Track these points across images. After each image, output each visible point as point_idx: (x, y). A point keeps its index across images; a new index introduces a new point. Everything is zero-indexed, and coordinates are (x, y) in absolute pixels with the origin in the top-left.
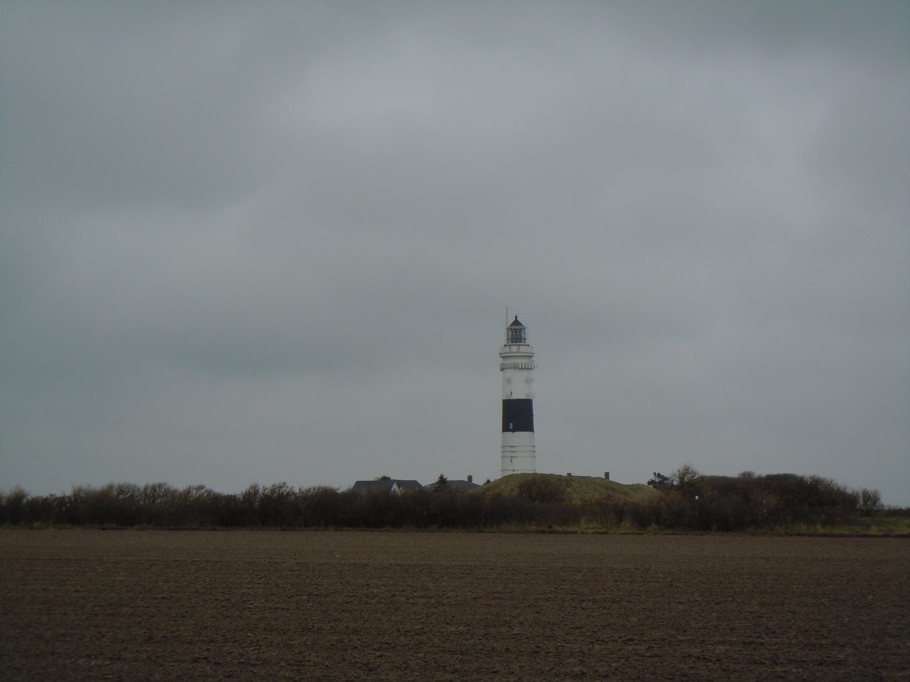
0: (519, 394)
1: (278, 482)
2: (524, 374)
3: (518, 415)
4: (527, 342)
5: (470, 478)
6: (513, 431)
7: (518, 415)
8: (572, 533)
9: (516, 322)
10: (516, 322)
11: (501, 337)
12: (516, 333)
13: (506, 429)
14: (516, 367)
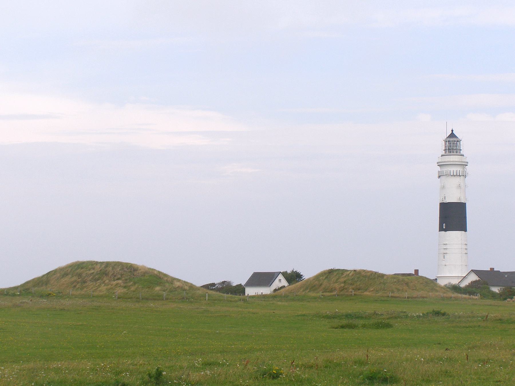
0: (452, 198)
1: (285, 271)
2: (456, 181)
3: (453, 217)
4: (462, 152)
5: (417, 271)
6: (445, 230)
7: (453, 217)
8: (386, 301)
9: (452, 135)
10: (452, 135)
11: (440, 147)
12: (452, 144)
13: (441, 229)
14: (449, 175)
